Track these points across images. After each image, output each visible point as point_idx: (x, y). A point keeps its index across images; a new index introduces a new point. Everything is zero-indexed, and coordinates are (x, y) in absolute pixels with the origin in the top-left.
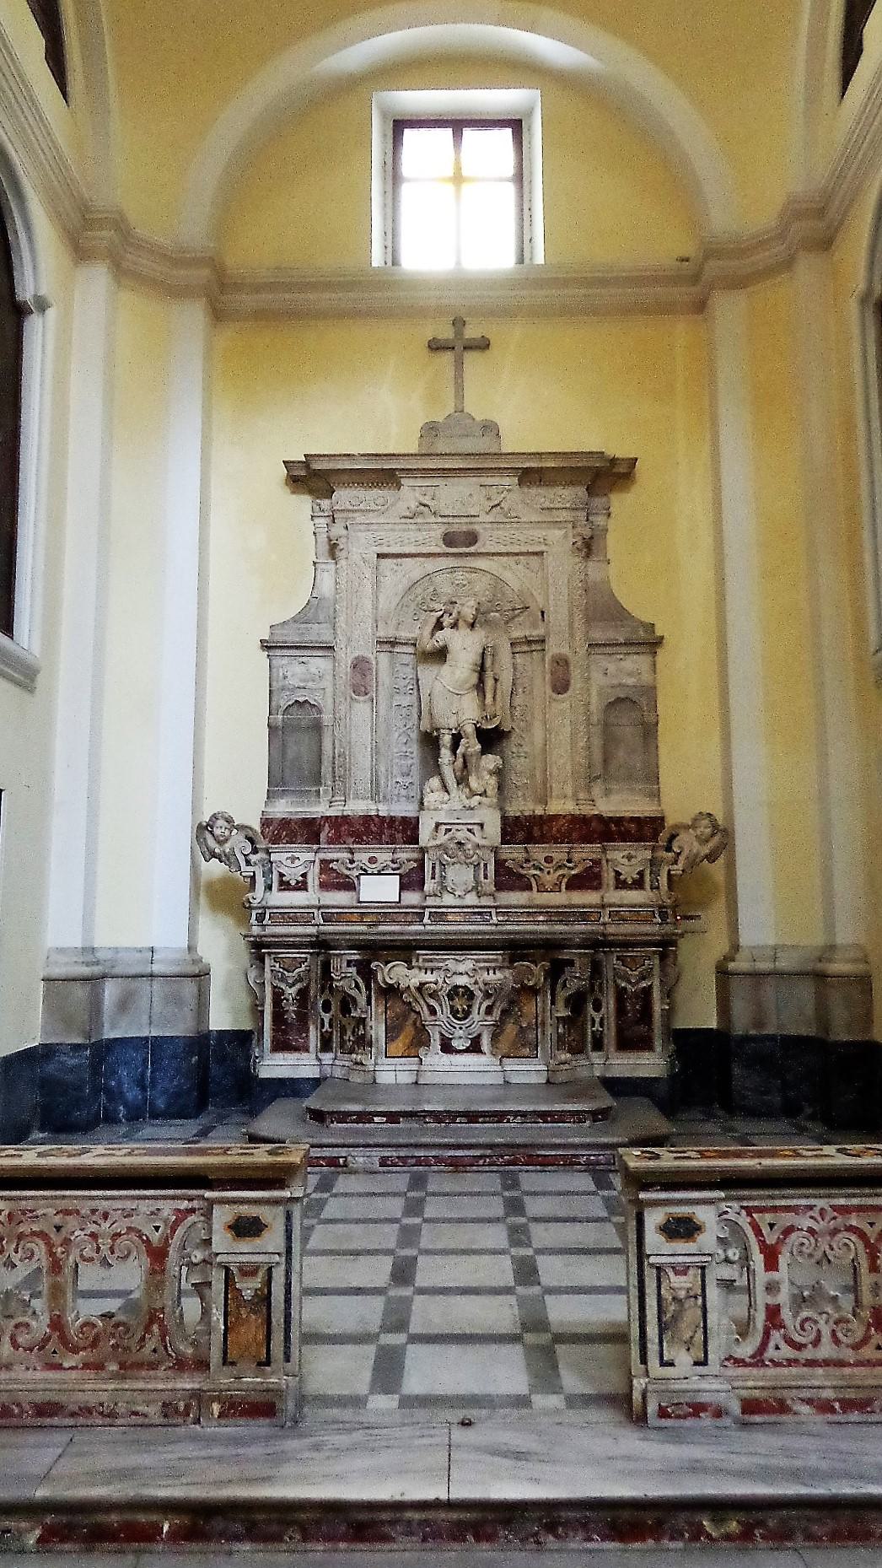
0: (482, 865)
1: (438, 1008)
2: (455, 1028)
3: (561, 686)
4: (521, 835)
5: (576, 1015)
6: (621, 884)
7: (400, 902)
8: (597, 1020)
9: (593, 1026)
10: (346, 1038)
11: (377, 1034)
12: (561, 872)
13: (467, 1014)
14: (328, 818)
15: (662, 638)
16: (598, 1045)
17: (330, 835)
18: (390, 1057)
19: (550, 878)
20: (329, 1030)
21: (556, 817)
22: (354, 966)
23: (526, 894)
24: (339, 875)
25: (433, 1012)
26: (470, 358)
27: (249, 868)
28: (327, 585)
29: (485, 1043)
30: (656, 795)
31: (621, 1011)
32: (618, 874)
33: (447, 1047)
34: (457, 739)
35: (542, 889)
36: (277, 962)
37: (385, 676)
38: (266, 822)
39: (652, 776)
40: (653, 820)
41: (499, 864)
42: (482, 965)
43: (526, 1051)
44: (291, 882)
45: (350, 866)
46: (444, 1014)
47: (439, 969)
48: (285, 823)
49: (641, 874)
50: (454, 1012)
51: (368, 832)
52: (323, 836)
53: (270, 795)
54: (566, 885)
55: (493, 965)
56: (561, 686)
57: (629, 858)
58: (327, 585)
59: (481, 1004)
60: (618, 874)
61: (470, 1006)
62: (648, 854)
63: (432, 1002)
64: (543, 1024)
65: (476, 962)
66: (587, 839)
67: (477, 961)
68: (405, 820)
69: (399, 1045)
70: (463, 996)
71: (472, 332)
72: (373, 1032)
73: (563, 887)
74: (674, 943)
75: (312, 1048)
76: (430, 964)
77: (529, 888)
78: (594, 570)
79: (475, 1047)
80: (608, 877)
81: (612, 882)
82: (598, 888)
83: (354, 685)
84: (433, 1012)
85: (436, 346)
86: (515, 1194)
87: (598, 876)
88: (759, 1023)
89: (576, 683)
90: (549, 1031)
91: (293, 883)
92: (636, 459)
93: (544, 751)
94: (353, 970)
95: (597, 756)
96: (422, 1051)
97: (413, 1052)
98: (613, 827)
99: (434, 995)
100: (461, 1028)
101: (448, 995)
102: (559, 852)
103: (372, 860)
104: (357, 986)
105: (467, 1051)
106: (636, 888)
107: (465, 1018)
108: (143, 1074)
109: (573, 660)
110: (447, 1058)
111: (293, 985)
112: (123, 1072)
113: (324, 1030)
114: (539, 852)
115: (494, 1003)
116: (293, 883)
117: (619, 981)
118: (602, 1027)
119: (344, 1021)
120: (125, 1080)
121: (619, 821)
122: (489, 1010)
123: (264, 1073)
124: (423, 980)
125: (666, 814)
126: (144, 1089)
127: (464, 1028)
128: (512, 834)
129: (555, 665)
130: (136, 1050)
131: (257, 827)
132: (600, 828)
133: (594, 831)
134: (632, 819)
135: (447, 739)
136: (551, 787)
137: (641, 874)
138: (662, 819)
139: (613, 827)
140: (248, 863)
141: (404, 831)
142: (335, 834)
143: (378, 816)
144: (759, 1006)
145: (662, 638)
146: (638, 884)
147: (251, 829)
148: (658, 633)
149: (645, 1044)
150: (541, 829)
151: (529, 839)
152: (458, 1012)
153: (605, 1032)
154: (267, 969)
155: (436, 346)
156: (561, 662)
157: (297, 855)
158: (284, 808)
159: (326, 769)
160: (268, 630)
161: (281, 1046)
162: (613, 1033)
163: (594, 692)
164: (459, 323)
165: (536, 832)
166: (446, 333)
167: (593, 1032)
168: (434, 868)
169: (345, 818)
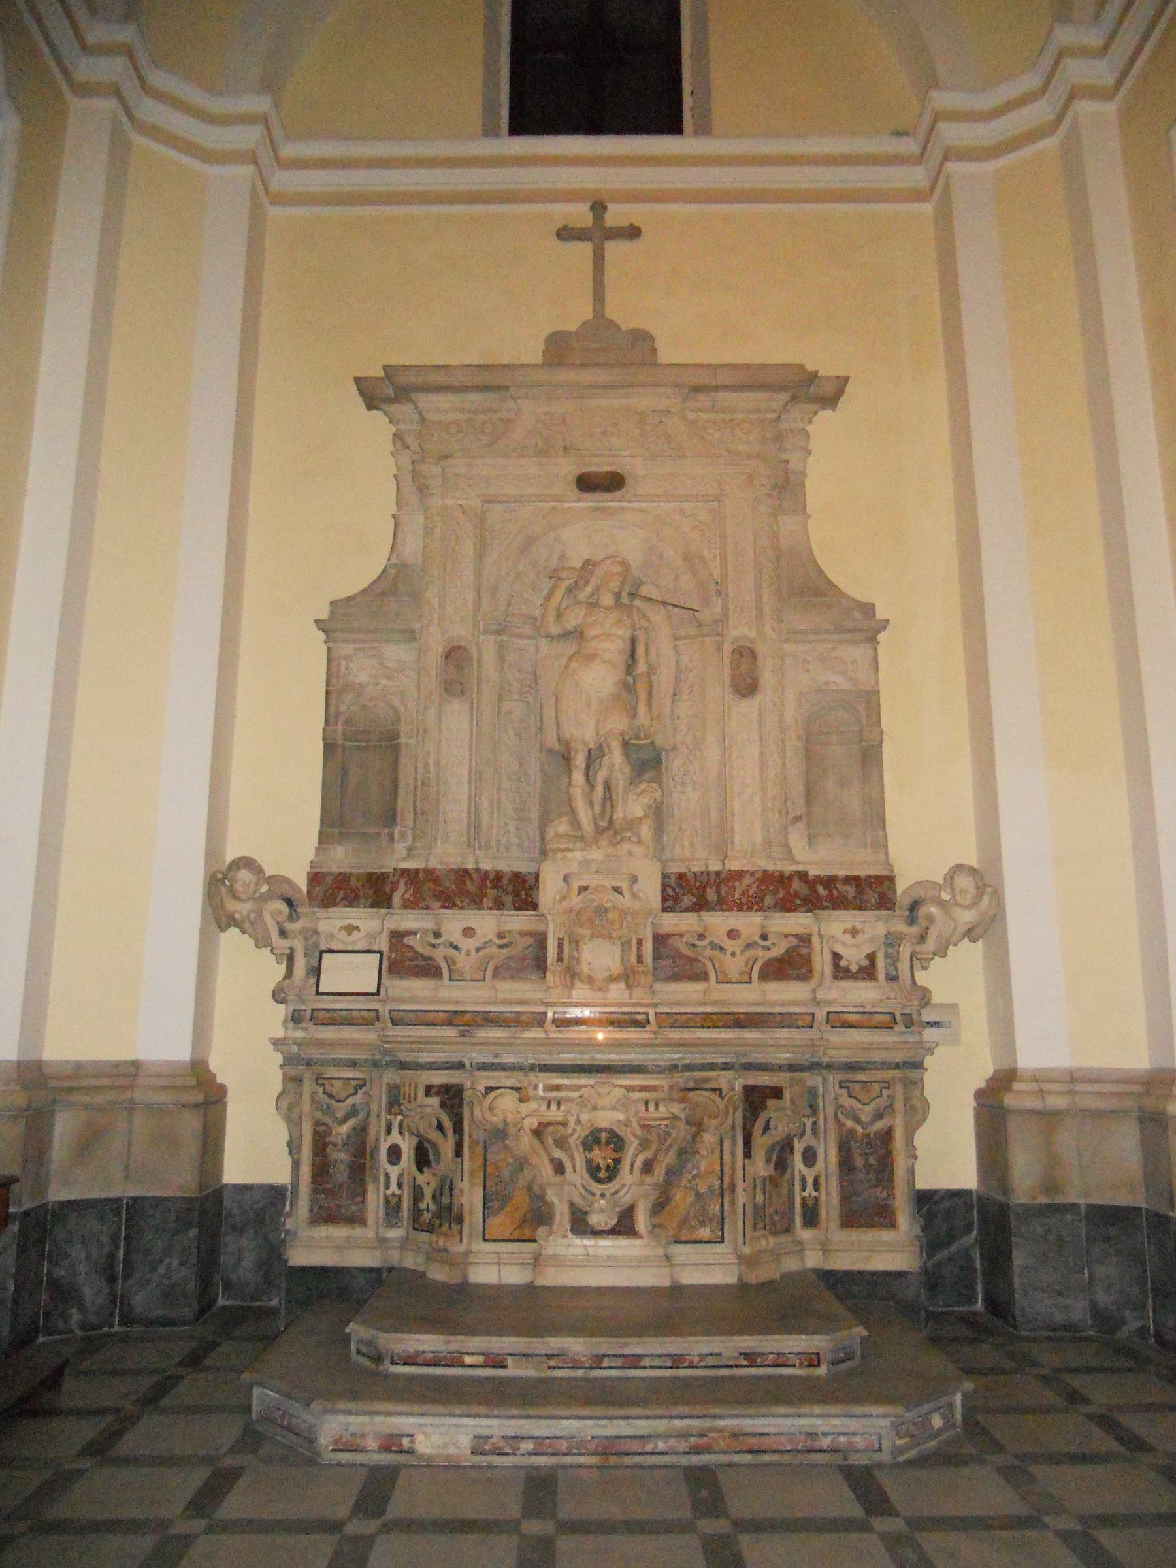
0: (634, 942)
1: (568, 1165)
2: (593, 1194)
3: (746, 687)
4: (687, 901)
5: (779, 1171)
6: (841, 972)
7: (380, 953)
8: (810, 1181)
9: (803, 1188)
10: (423, 1206)
11: (471, 1205)
12: (750, 953)
13: (613, 1172)
14: (404, 872)
15: (887, 621)
16: (811, 1218)
17: (407, 896)
18: (488, 1241)
19: (734, 966)
20: (398, 1192)
21: (738, 875)
22: (437, 1094)
23: (700, 986)
24: (418, 956)
25: (559, 1168)
26: (613, 249)
27: (286, 944)
28: (412, 548)
29: (642, 1220)
30: (881, 844)
31: (846, 1165)
32: (837, 957)
33: (580, 1225)
34: (594, 756)
35: (724, 980)
36: (321, 1085)
37: (490, 669)
38: (315, 878)
39: (876, 818)
40: (880, 880)
41: (660, 940)
42: (637, 1095)
43: (705, 1232)
44: (851, 967)
45: (434, 941)
46: (577, 1175)
47: (570, 1100)
48: (342, 879)
49: (871, 957)
50: (593, 1170)
51: (463, 893)
52: (397, 899)
53: (324, 838)
54: (761, 970)
55: (654, 1095)
56: (746, 687)
57: (854, 932)
58: (412, 548)
59: (635, 1156)
60: (837, 957)
61: (617, 1161)
62: (881, 929)
63: (558, 1154)
64: (733, 1188)
65: (628, 1091)
66: (786, 906)
67: (629, 1089)
68: (517, 877)
69: (500, 1223)
70: (608, 1143)
71: (616, 215)
72: (464, 1200)
73: (755, 976)
74: (918, 1065)
75: (371, 1219)
76: (555, 1094)
77: (703, 977)
78: (788, 524)
79: (624, 1227)
80: (822, 963)
81: (828, 970)
82: (806, 976)
83: (445, 682)
84: (559, 1168)
85: (565, 234)
86: (721, 1526)
87: (807, 961)
88: (1051, 1185)
89: (767, 679)
90: (742, 1198)
91: (854, 968)
92: (847, 379)
93: (721, 775)
94: (434, 1101)
95: (797, 788)
96: (541, 1231)
97: (527, 1232)
98: (821, 891)
99: (561, 1143)
100: (603, 1195)
101: (584, 1144)
102: (749, 923)
103: (468, 932)
104: (440, 1127)
105: (614, 1232)
106: (864, 979)
107: (610, 1179)
108: (112, 1256)
109: (761, 649)
110: (582, 1245)
111: (345, 1119)
112: (77, 1253)
113: (389, 1192)
114: (718, 922)
115: (656, 1154)
116: (854, 968)
117: (843, 1119)
118: (816, 1190)
119: (421, 1179)
120: (82, 1268)
121: (829, 882)
122: (648, 1168)
123: (299, 1257)
124: (546, 1119)
125: (897, 870)
126: (112, 1279)
127: (608, 1196)
128: (676, 899)
129: (737, 656)
130: (102, 1218)
131: (303, 885)
132: (804, 890)
133: (796, 895)
134: (848, 880)
135: (580, 760)
136: (732, 828)
137: (871, 957)
138: (891, 879)
139: (821, 891)
140: (283, 933)
141: (516, 894)
142: (415, 894)
143: (477, 870)
144: (1052, 1161)
145: (887, 621)
146: (868, 972)
147: (288, 881)
148: (880, 615)
149: (882, 1216)
150: (718, 892)
151: (700, 905)
152: (598, 1168)
153: (823, 1197)
154: (306, 1098)
155: (565, 234)
156: (745, 654)
157: (355, 923)
158: (341, 858)
159: (404, 802)
160: (327, 608)
161: (324, 1216)
162: (835, 1200)
163: (790, 695)
164: (598, 208)
165: (711, 895)
166: (580, 213)
167: (804, 1199)
168: (560, 946)
169: (429, 872)
